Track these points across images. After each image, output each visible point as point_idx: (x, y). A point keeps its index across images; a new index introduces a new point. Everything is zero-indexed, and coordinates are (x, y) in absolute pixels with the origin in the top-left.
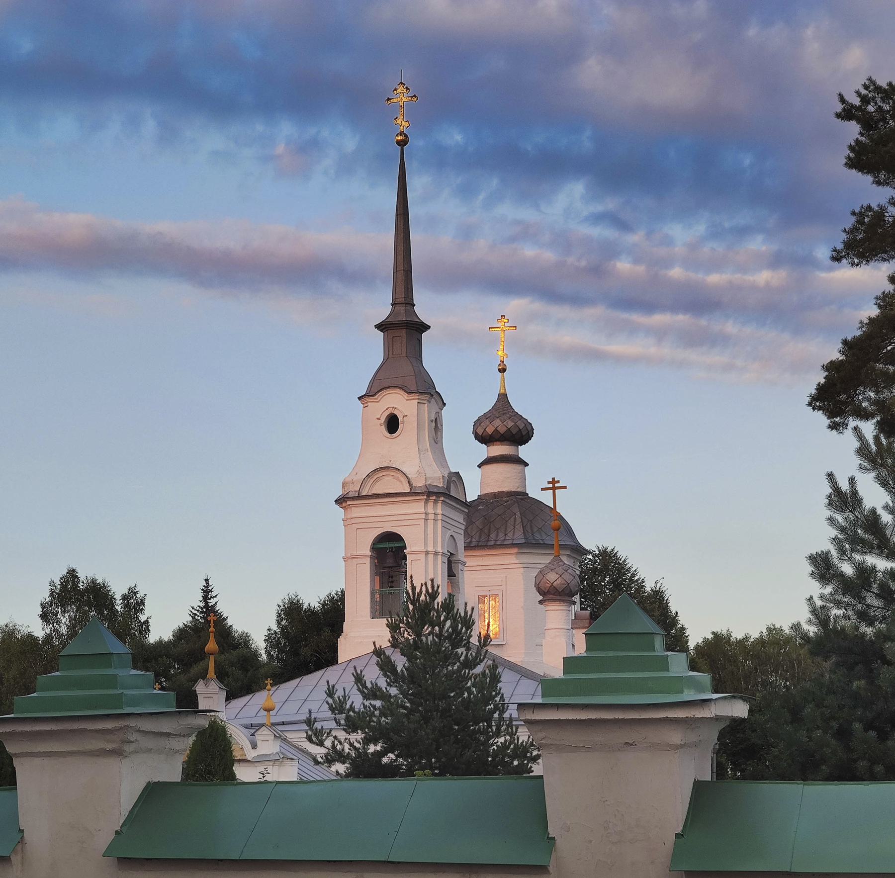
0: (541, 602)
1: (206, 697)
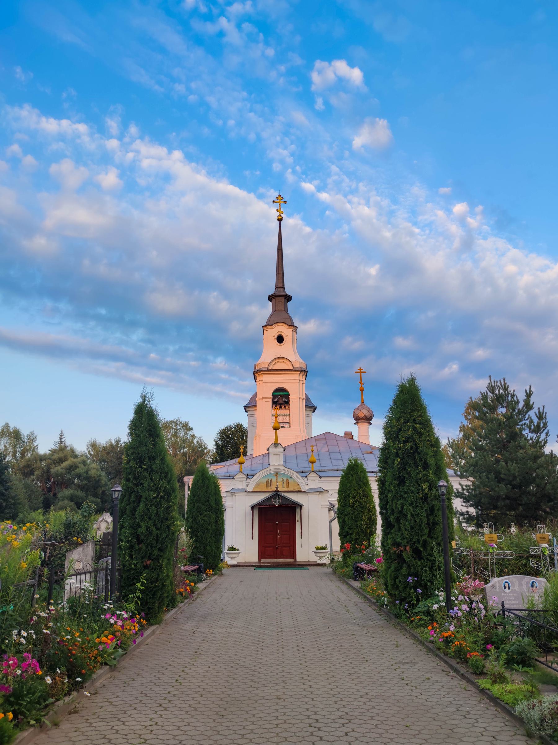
0: (355, 424)
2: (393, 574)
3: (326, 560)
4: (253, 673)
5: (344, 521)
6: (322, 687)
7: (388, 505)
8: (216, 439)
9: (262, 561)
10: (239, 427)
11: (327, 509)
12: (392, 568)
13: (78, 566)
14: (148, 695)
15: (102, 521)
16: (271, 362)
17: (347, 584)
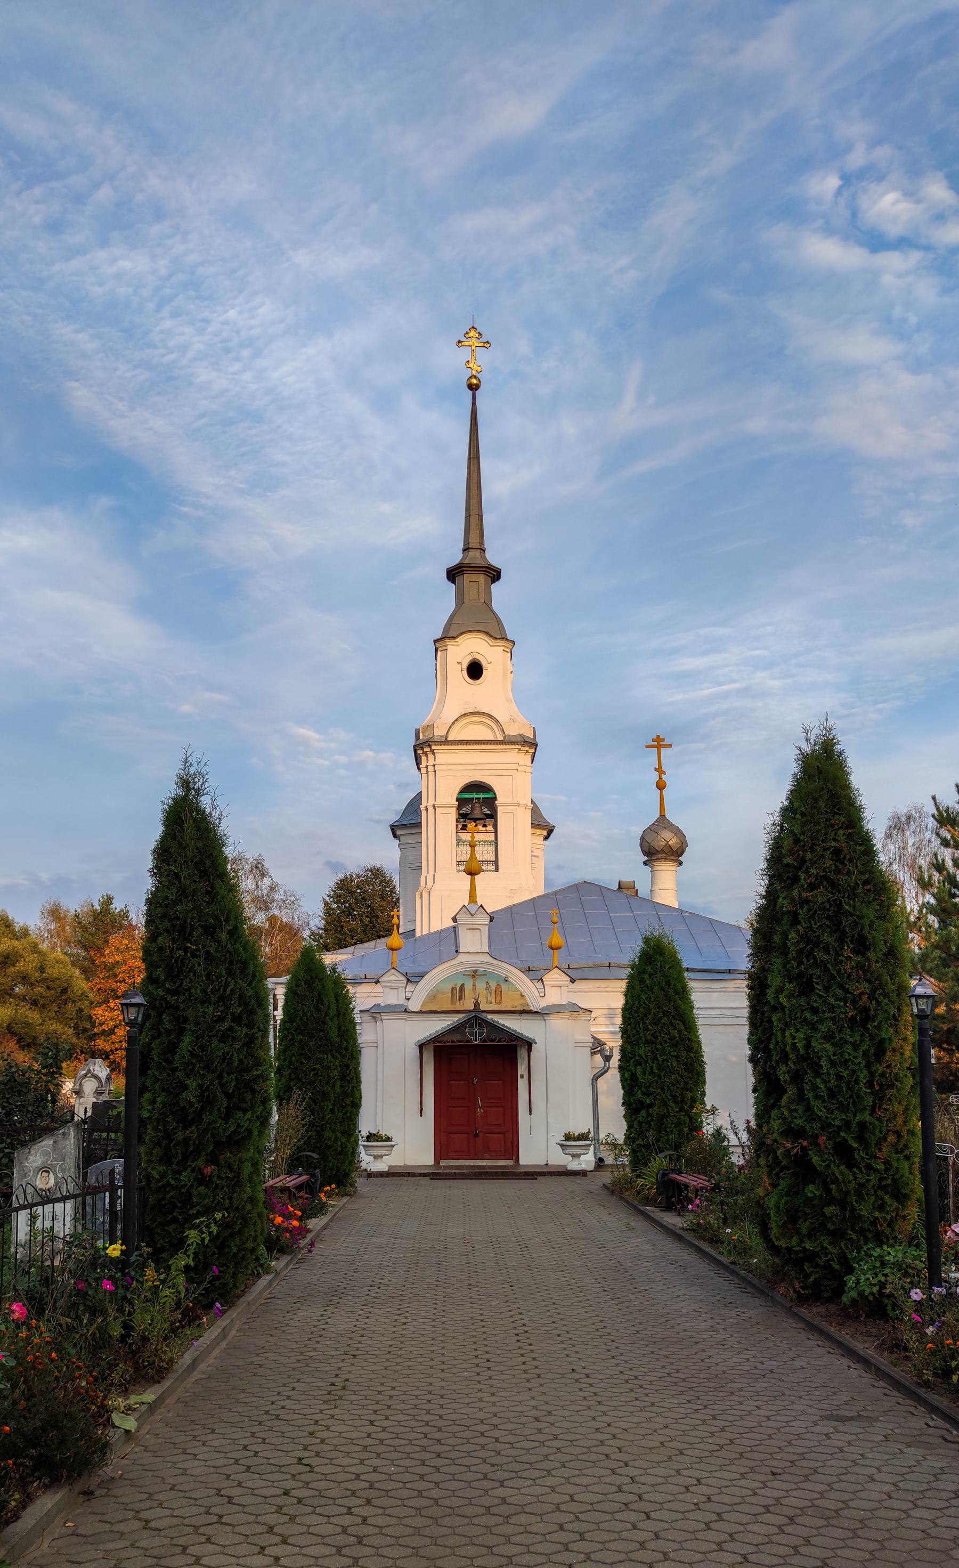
0: (645, 863)
1: (469, 929)
2: (783, 1201)
3: (587, 1161)
4: (483, 1441)
5: (634, 1077)
6: (662, 1480)
7: (773, 1041)
8: (327, 898)
9: (443, 1163)
10: (376, 874)
11: (589, 1050)
12: (780, 1188)
13: (46, 1182)
14: (236, 1500)
15: (85, 1075)
16: (453, 723)
17: (647, 1217)
